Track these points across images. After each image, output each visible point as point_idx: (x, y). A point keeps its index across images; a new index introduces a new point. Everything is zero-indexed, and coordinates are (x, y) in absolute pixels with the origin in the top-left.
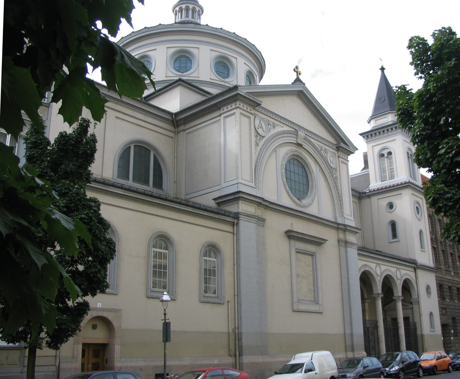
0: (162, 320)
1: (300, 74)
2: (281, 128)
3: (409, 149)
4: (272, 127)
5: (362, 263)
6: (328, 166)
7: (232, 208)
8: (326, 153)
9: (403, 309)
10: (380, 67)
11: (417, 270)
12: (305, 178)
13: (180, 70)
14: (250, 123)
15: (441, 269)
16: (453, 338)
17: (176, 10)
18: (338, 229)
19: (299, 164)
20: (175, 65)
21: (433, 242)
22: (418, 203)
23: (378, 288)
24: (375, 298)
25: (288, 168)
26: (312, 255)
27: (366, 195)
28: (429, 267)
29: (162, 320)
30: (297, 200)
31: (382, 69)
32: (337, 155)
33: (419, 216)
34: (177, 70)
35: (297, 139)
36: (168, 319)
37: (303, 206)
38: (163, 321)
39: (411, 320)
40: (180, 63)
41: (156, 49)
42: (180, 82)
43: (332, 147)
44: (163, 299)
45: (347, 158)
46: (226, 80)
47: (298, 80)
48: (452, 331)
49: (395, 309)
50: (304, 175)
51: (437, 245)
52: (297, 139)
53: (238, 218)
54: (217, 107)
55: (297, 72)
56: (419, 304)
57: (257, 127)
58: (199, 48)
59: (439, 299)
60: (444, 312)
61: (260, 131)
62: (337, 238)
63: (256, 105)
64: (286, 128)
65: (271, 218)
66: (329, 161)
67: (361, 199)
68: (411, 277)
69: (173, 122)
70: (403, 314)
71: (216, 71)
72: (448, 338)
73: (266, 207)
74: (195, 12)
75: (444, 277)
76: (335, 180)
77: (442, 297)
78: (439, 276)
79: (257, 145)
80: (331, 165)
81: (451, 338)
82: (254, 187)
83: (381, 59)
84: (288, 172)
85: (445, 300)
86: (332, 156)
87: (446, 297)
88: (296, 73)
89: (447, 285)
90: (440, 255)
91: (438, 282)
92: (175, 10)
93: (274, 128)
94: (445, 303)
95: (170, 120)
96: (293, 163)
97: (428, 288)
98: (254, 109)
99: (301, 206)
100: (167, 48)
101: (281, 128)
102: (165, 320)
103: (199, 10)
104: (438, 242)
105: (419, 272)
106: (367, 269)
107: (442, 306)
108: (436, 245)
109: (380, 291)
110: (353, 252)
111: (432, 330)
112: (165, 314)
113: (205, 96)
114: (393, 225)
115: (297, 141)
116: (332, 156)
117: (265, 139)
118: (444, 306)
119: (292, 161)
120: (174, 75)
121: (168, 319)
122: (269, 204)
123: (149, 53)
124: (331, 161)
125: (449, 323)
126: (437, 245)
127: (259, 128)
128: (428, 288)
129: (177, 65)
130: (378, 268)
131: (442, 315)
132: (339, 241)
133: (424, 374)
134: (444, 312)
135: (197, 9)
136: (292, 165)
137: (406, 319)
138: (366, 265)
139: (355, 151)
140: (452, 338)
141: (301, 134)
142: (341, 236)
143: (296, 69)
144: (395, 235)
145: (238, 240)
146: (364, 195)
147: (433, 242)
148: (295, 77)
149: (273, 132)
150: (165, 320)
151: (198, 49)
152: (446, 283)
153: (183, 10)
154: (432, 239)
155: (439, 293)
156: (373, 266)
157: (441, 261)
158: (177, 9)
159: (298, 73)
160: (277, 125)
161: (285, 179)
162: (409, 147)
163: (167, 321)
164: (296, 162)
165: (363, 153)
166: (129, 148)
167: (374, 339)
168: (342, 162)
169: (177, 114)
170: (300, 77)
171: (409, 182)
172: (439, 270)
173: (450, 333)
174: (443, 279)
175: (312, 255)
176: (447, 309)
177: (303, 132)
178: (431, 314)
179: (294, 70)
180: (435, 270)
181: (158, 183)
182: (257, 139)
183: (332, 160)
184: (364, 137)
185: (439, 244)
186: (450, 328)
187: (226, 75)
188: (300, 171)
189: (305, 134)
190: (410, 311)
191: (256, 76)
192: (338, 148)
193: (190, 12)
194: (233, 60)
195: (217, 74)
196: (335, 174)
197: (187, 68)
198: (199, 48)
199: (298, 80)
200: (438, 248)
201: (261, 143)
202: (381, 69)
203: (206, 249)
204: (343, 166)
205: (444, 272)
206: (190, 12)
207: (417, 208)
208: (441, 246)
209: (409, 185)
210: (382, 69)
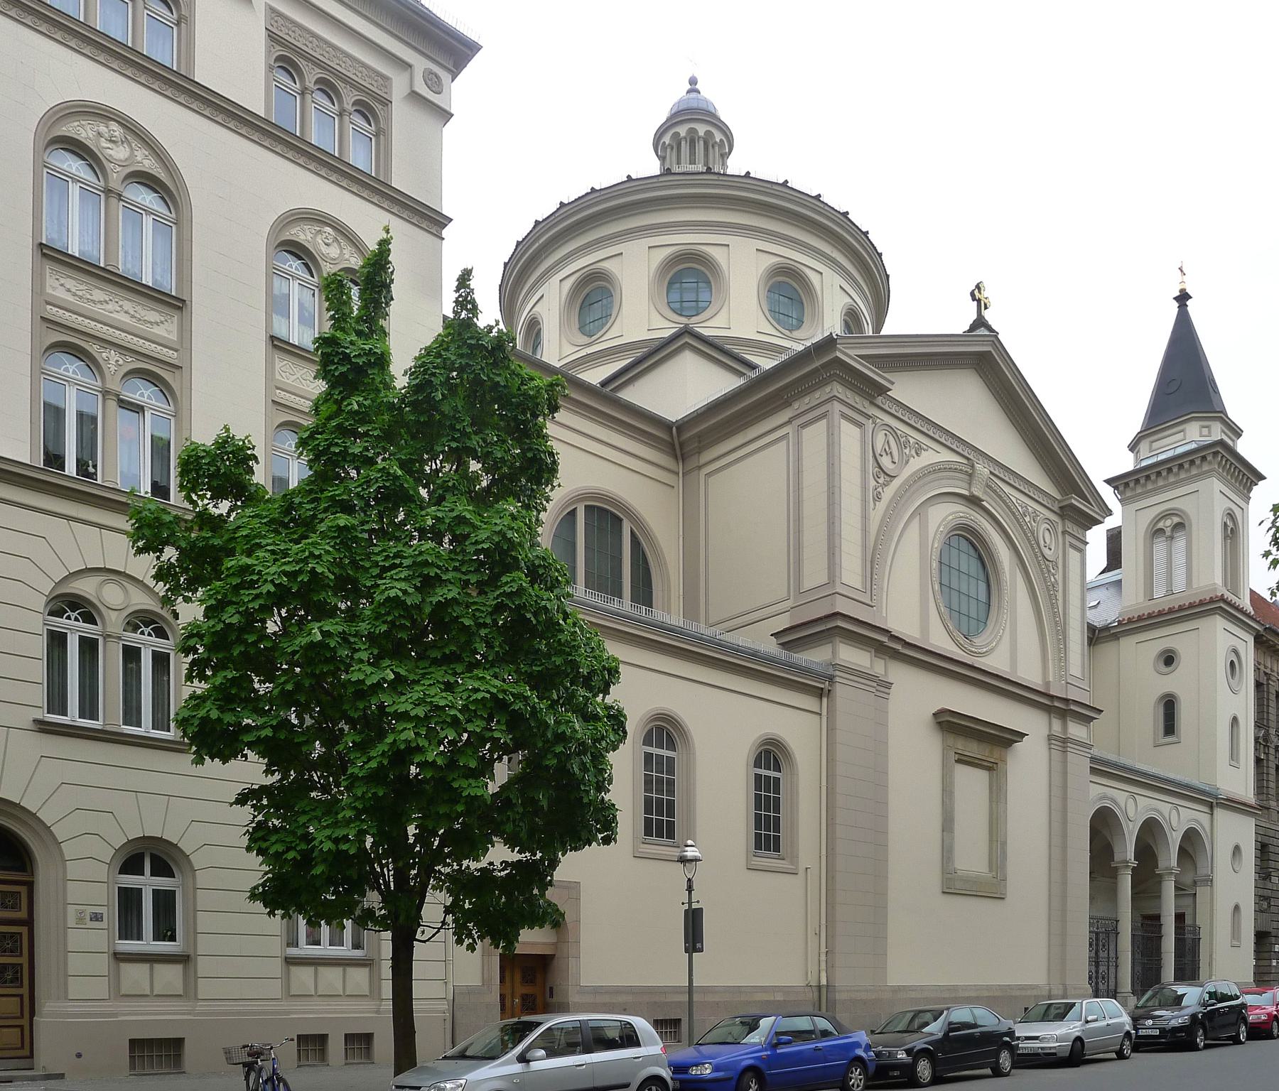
0: (683, 904)
1: (986, 308)
2: (935, 455)
4: (913, 452)
5: (1095, 791)
6: (1039, 554)
7: (815, 657)
8: (1034, 521)
11: (1215, 812)
12: (983, 586)
13: (682, 309)
14: (863, 442)
16: (1277, 963)
17: (664, 142)
18: (1048, 709)
19: (972, 551)
20: (670, 294)
22: (1235, 652)
23: (1127, 851)
24: (1116, 869)
25: (945, 560)
26: (989, 769)
28: (1245, 804)
29: (683, 904)
30: (961, 639)
31: (1183, 298)
32: (1060, 529)
34: (674, 311)
35: (970, 484)
36: (698, 902)
37: (976, 653)
38: (686, 906)
39: (1188, 921)
40: (682, 291)
41: (622, 253)
42: (686, 340)
43: (1050, 506)
44: (686, 856)
45: (1085, 537)
46: (796, 334)
47: (980, 322)
49: (1157, 896)
50: (982, 576)
51: (1267, 754)
52: (970, 484)
53: (831, 679)
54: (782, 401)
55: (979, 301)
56: (1211, 886)
58: (728, 245)
60: (1265, 905)
61: (886, 461)
62: (1047, 733)
63: (874, 391)
64: (946, 456)
65: (903, 678)
66: (1042, 543)
68: (1201, 825)
69: (672, 445)
71: (770, 310)
72: (1265, 963)
73: (896, 655)
74: (713, 147)
76: (1051, 589)
77: (1264, 873)
79: (878, 498)
80: (1046, 551)
82: (870, 603)
83: (1181, 269)
84: (945, 569)
86: (1048, 529)
87: (1273, 874)
88: (976, 302)
90: (1271, 710)
91: (1260, 840)
92: (662, 141)
93: (917, 454)
94: (1270, 886)
95: (663, 440)
96: (956, 546)
98: (872, 403)
99: (971, 653)
100: (649, 248)
101: (935, 455)
102: (690, 903)
103: (721, 140)
106: (1108, 804)
107: (1261, 892)
109: (1130, 854)
110: (1079, 764)
111: (1235, 943)
112: (690, 889)
113: (741, 374)
114: (1169, 706)
115: (970, 491)
116: (1048, 529)
117: (896, 483)
118: (1268, 893)
119: (954, 542)
120: (665, 327)
121: (698, 902)
122: (902, 647)
123: (605, 265)
124: (1045, 542)
125: (1271, 930)
126: (1267, 754)
127: (884, 454)
129: (675, 296)
130: (1131, 801)
131: (1259, 911)
132: (1050, 737)
133: (135, 935)
134: (1265, 905)
135: (718, 136)
136: (954, 552)
137: (1180, 918)
138: (1104, 797)
139: (1105, 518)
141: (982, 469)
142: (1057, 726)
143: (976, 292)
144: (1170, 727)
145: (831, 729)
148: (974, 316)
149: (916, 464)
150: (690, 903)
151: (726, 248)
153: (683, 143)
154: (1256, 740)
156: (1121, 797)
158: (667, 139)
159: (981, 304)
160: (925, 447)
161: (937, 587)
162: (1231, 509)
163: (694, 906)
164: (964, 543)
165: (1108, 531)
166: (573, 513)
167: (1108, 958)
168: (1072, 546)
169: (683, 425)
170: (987, 315)
171: (1222, 599)
172: (1266, 811)
175: (990, 768)
177: (986, 466)
179: (972, 294)
180: (1258, 810)
181: (644, 593)
182: (878, 482)
183: (1048, 541)
184: (1116, 488)
187: (795, 322)
188: (972, 566)
189: (991, 472)
190: (1189, 901)
191: (868, 324)
192: (1067, 512)
193: (700, 147)
194: (814, 278)
195: (774, 318)
196: (1053, 575)
197: (701, 304)
198: (728, 245)
199: (980, 322)
200: (1268, 760)
201: (888, 493)
203: (759, 751)
204: (1073, 555)
205: (1274, 816)
206: (700, 147)
207: (1232, 663)
210: (1183, 298)
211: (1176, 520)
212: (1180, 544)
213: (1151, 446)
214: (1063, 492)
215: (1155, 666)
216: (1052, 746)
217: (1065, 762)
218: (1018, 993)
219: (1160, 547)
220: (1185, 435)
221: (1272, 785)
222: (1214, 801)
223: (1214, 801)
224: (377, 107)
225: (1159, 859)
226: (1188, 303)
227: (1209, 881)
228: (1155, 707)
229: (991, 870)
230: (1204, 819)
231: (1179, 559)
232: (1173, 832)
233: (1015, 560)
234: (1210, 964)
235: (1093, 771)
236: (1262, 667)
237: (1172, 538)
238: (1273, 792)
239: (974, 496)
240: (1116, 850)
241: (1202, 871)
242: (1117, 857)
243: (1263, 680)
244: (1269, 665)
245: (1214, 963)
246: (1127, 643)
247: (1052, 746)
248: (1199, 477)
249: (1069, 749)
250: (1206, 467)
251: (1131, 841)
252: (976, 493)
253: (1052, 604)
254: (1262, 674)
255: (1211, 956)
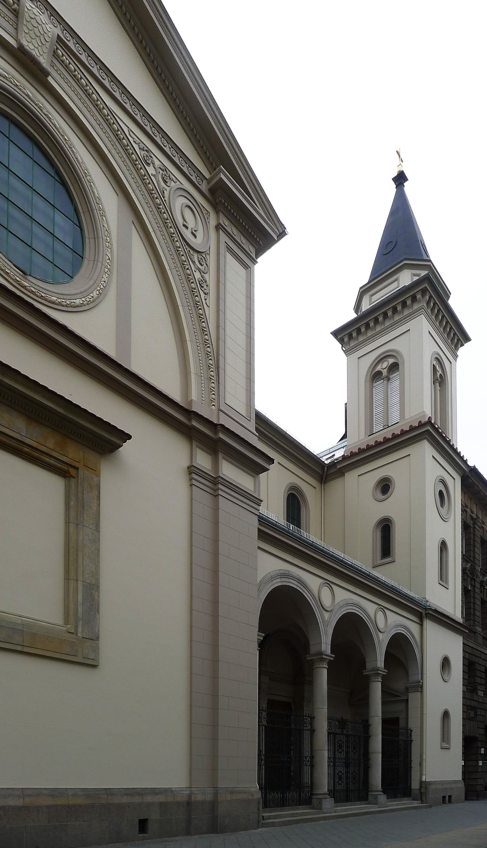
3: (437, 358)
9: (383, 703)
10: (395, 174)
15: (475, 633)
16: (483, 763)
21: (466, 578)
22: (443, 482)
27: (335, 470)
33: (443, 511)
48: (483, 751)
51: (474, 586)
56: (422, 692)
57: (35, 255)
58: (441, 748)
59: (465, 687)
67: (325, 483)
70: (383, 713)
75: (480, 649)
78: (471, 645)
81: (478, 763)
85: (477, 693)
86: (188, 206)
89: (483, 666)
90: (477, 550)
97: (446, 663)
104: (475, 580)
105: (430, 626)
107: (468, 703)
108: (471, 585)
111: (445, 745)
116: (188, 206)
118: (473, 704)
126: (474, 586)
128: (446, 663)
131: (467, 719)
134: (472, 714)
138: (286, 575)
140: (481, 763)
146: (332, 471)
147: (466, 578)
152: (481, 661)
154: (464, 570)
155: (466, 677)
157: (476, 562)
162: (439, 354)
173: (478, 753)
174: (478, 653)
176: (478, 710)
178: (446, 715)
185: (478, 585)
186: (480, 744)
202: (395, 179)
205: (480, 640)
207: (441, 492)
208: (481, 592)
209: (405, 264)
211: (391, 361)
212: (395, 384)
213: (370, 299)
214: (212, 166)
215: (374, 496)
216: (194, 482)
217: (216, 509)
218: (125, 800)
219: (379, 385)
220: (398, 284)
221: (478, 614)
222: (424, 612)
223: (424, 612)
224: (72, 471)
225: (367, 660)
226: (405, 184)
227: (419, 687)
228: (373, 532)
229: (67, 622)
230: (414, 628)
231: (395, 399)
232: (379, 633)
233: (129, 216)
234: (421, 764)
235: (262, 535)
236: (468, 510)
237: (389, 379)
238: (479, 620)
239: (21, 48)
240: (311, 642)
241: (413, 678)
242: (313, 649)
243: (471, 523)
244: (475, 510)
245: (424, 763)
246: (351, 477)
247: (194, 482)
248: (411, 317)
249: (220, 492)
250: (416, 306)
251: (326, 634)
252: (29, 46)
253: (200, 316)
254: (469, 517)
255: (421, 756)
